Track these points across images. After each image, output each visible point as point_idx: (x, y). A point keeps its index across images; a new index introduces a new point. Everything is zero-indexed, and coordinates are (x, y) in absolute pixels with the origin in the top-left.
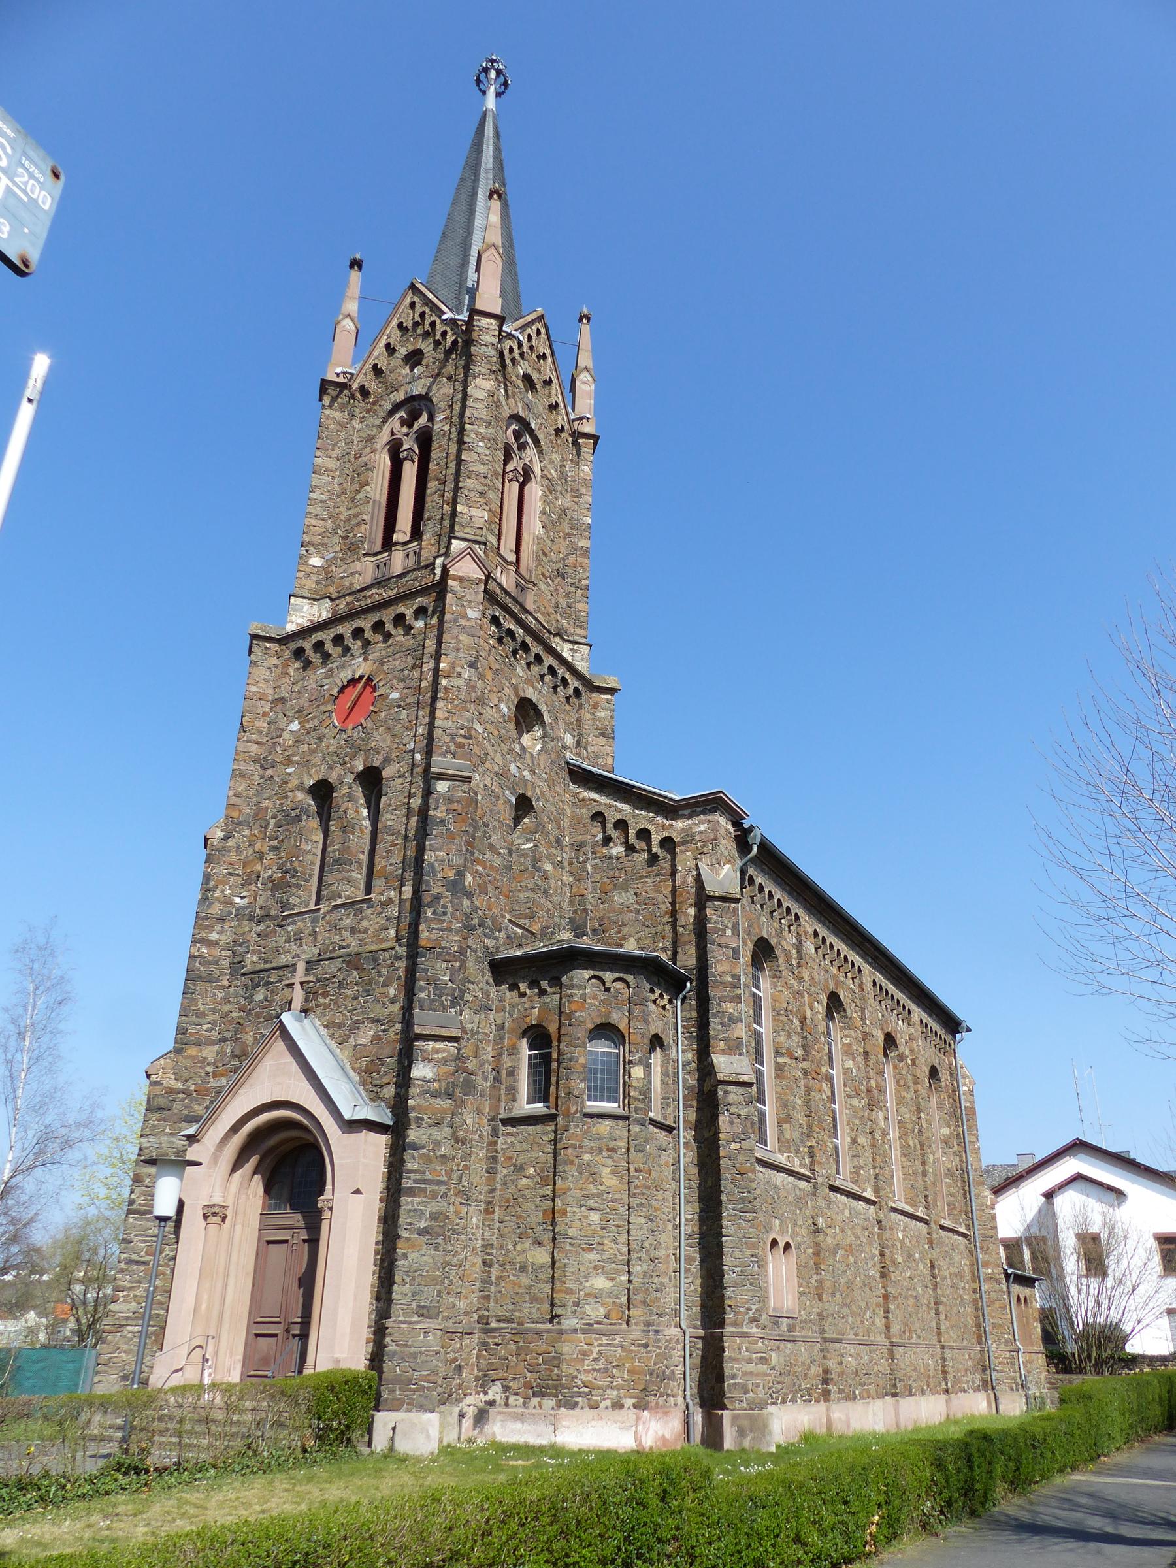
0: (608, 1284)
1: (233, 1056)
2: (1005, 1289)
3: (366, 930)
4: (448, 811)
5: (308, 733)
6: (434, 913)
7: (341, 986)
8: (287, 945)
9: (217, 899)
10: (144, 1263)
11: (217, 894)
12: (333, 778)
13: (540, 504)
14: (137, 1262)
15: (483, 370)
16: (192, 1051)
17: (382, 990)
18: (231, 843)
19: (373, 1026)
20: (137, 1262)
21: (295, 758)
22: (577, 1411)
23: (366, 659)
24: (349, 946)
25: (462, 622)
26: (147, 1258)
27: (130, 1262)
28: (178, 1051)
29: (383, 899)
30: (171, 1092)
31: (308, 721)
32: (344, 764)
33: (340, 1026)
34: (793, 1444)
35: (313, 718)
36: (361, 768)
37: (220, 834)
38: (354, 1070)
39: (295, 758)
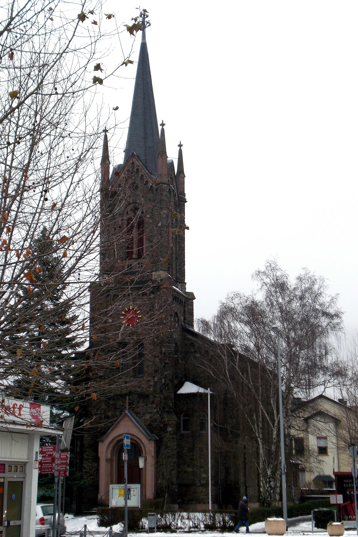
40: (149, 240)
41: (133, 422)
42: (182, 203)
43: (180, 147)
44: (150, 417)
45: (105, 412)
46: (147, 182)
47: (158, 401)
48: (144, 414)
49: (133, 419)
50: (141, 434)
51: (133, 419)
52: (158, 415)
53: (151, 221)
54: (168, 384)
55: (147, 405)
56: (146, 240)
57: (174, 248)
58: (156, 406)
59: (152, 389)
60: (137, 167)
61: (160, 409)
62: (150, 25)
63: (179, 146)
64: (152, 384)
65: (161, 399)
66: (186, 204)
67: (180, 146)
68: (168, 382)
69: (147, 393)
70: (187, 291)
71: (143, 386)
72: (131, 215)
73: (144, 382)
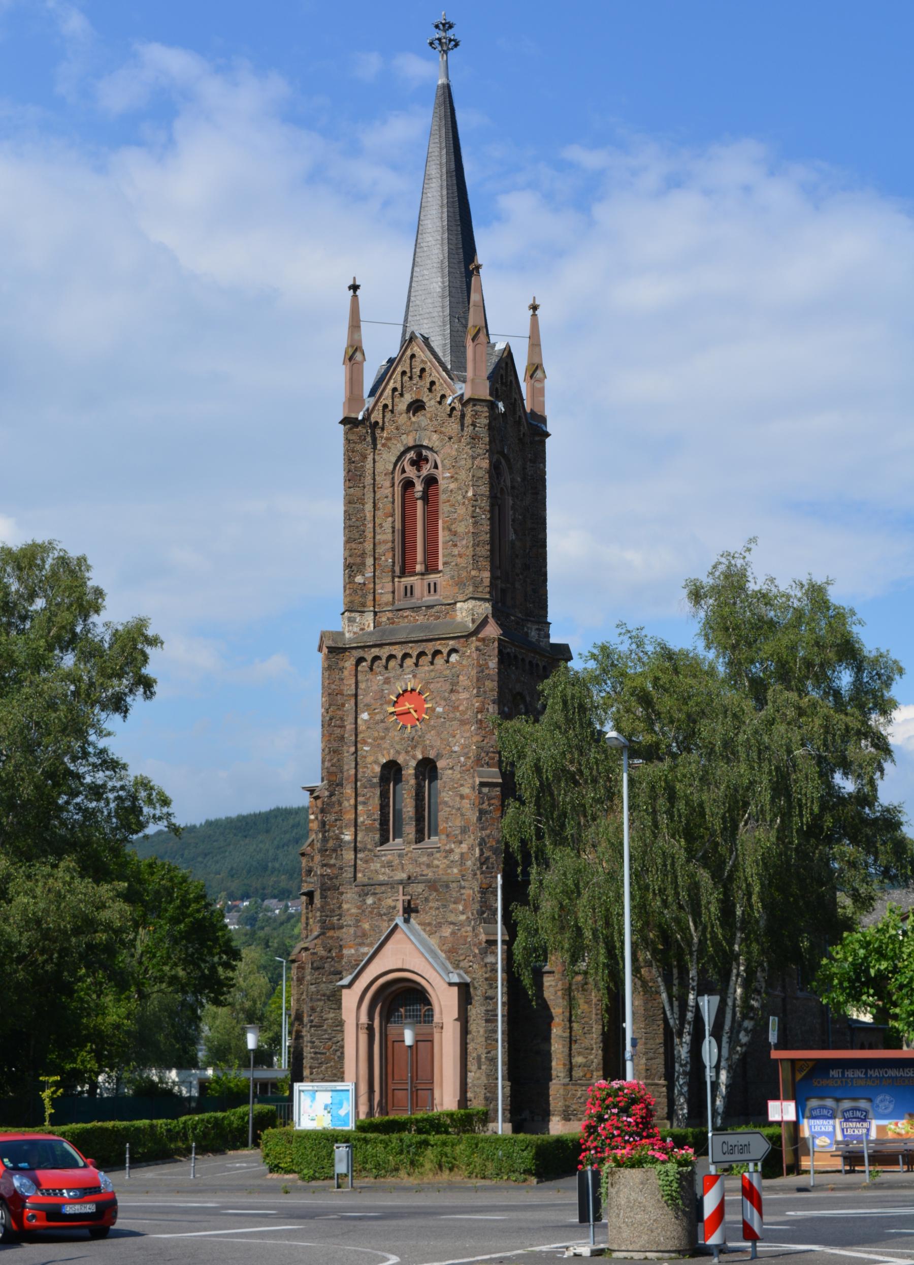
0: (584, 1060)
1: (356, 936)
2: (849, 1039)
3: (438, 867)
4: (490, 805)
5: (377, 723)
6: (487, 868)
7: (427, 900)
8: (383, 870)
9: (331, 837)
10: (323, 1054)
11: (331, 834)
12: (400, 760)
13: (511, 512)
14: (320, 1053)
15: (481, 451)
16: (330, 933)
17: (454, 906)
18: (334, 799)
19: (451, 926)
20: (320, 1053)
21: (370, 740)
22: (571, 1122)
23: (414, 676)
24: (427, 875)
25: (487, 672)
26: (324, 1051)
27: (316, 1053)
28: (323, 933)
29: (447, 848)
30: (322, 958)
31: (376, 714)
32: (407, 752)
33: (430, 924)
34: (844, 609)
35: (378, 713)
36: (420, 757)
37: (327, 793)
38: (442, 951)
39: (370, 740)
40: (450, 530)
41: (413, 943)
42: (537, 439)
43: (355, 292)
44: (453, 933)
45: (358, 921)
46: (443, 397)
47: (469, 895)
48: (439, 925)
49: (412, 937)
50: (431, 970)
51: (412, 937)
52: (469, 929)
53: (452, 486)
54: (488, 858)
55: (445, 906)
56: (443, 529)
57: (518, 544)
58: (465, 907)
59: (455, 871)
60: (422, 366)
61: (472, 914)
62: (456, 45)
63: (350, 288)
64: (457, 857)
65: (474, 893)
66: (548, 440)
67: (534, 308)
68: (487, 854)
69: (445, 878)
70: (144, 671)
71: (436, 862)
72: (411, 472)
73: (438, 855)
